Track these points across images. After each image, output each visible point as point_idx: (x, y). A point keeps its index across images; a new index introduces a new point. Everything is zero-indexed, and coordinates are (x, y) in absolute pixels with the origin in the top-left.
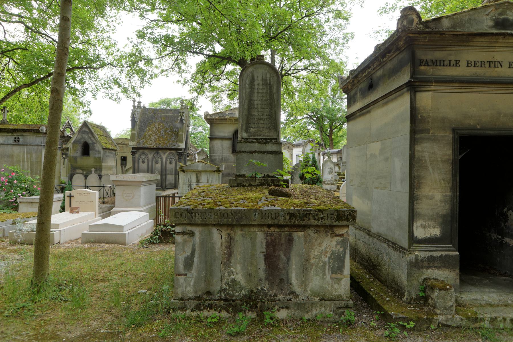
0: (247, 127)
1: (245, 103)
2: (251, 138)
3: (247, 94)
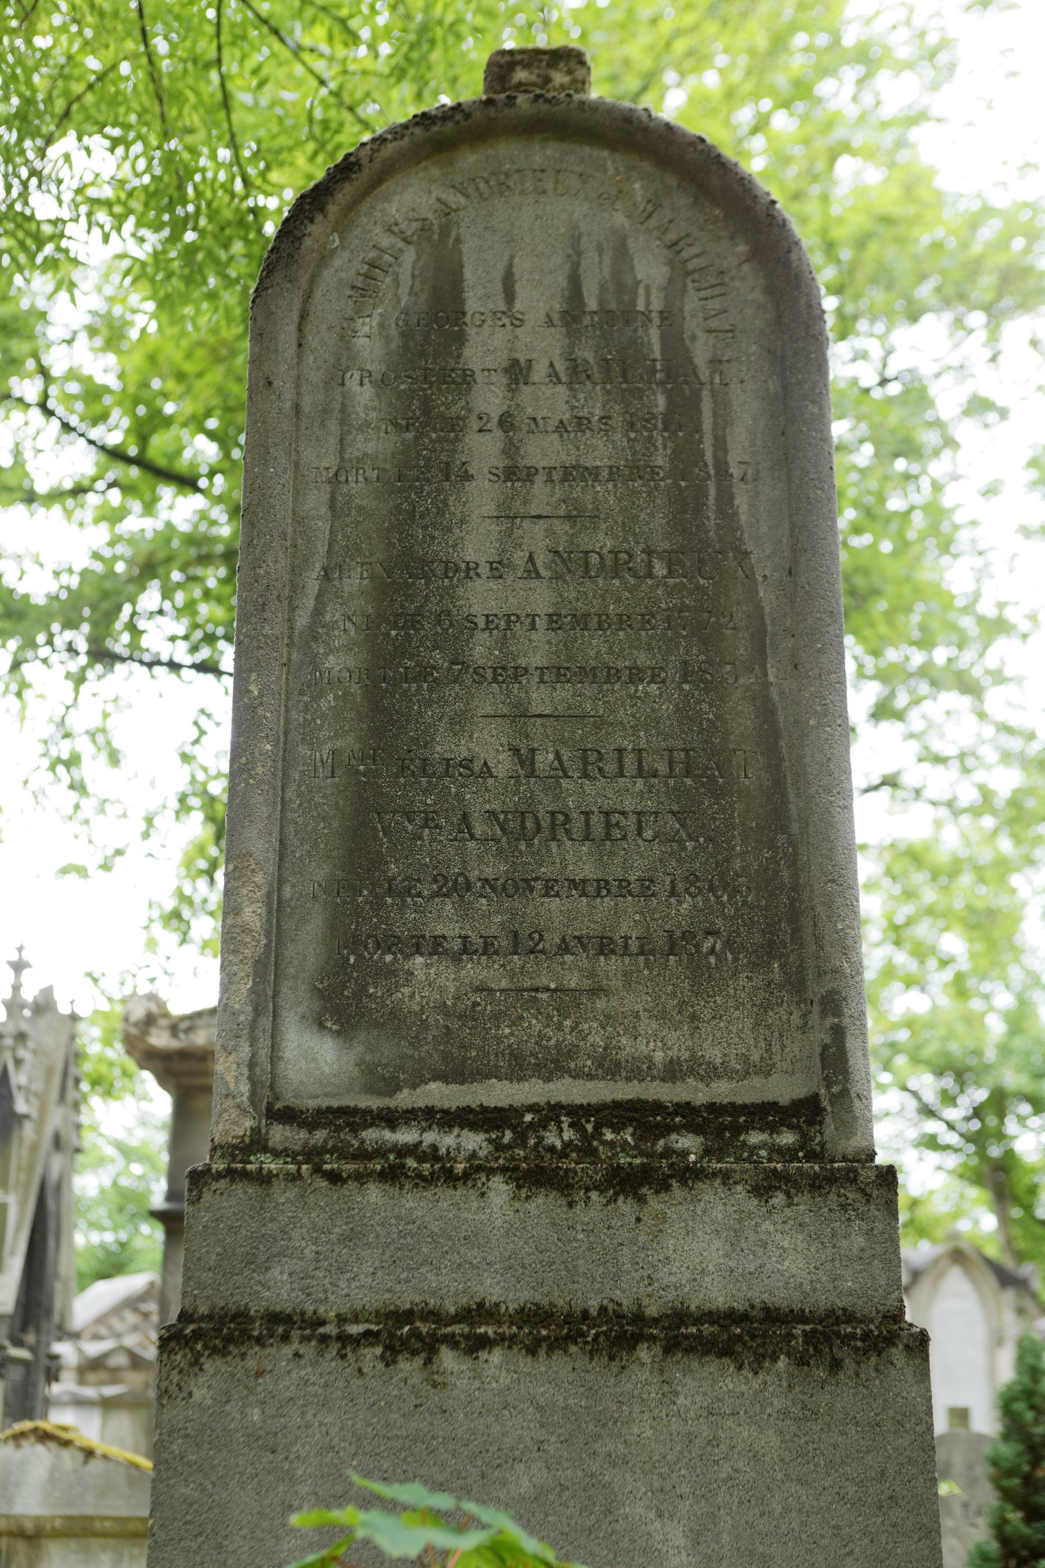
0: (356, 942)
1: (333, 613)
2: (404, 1099)
3: (355, 487)
